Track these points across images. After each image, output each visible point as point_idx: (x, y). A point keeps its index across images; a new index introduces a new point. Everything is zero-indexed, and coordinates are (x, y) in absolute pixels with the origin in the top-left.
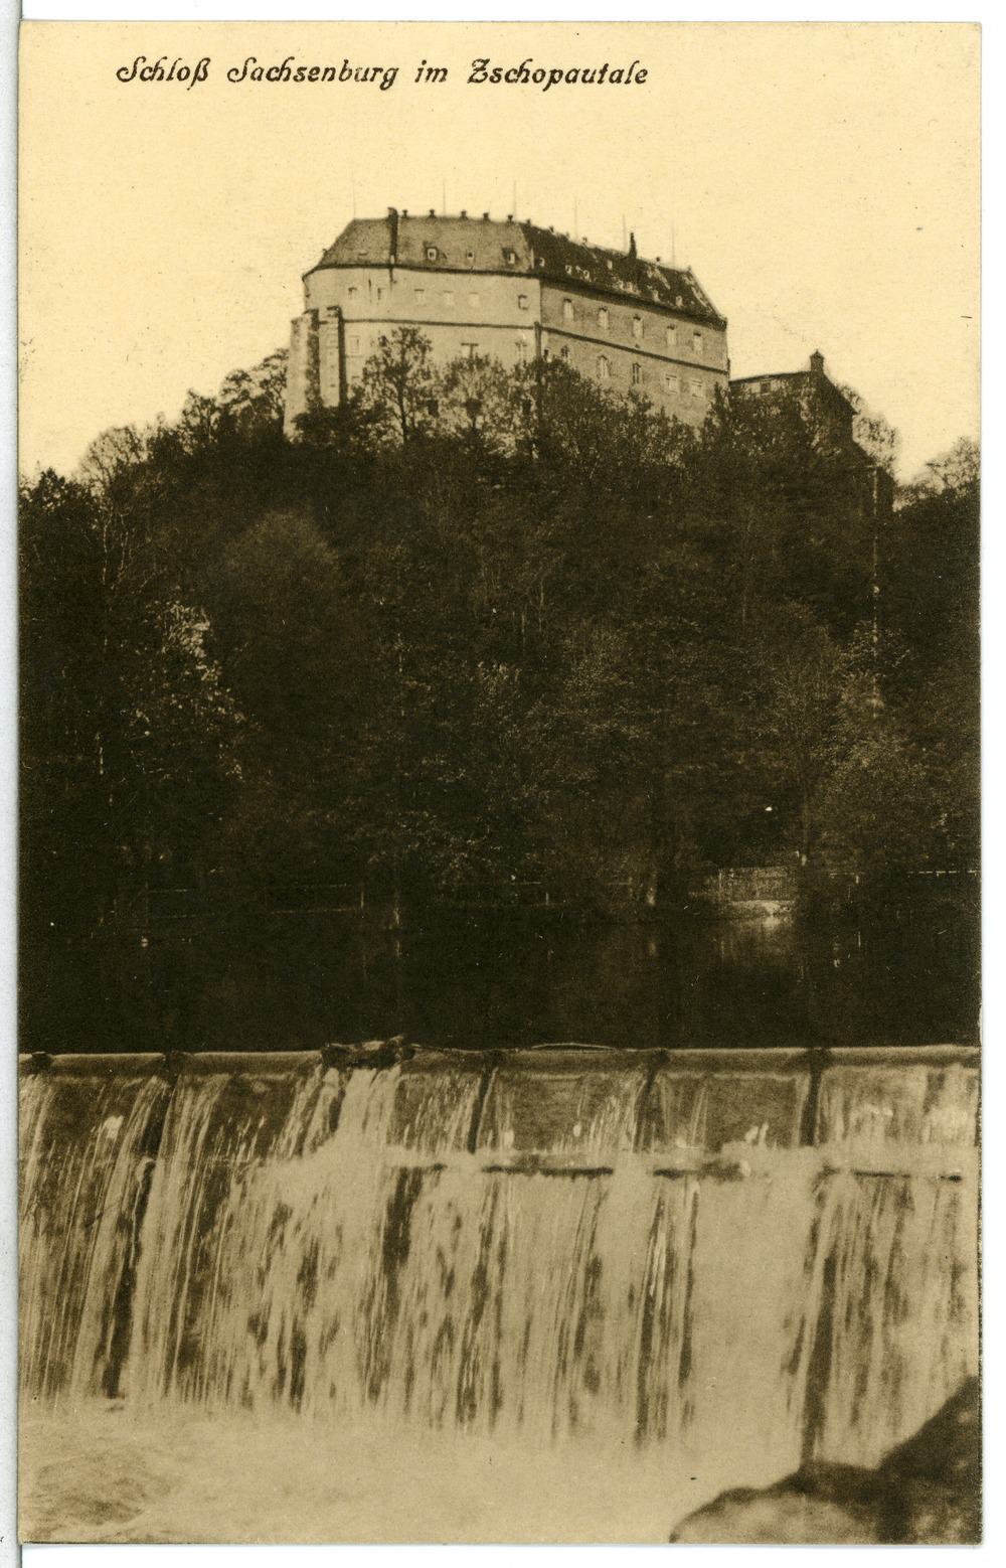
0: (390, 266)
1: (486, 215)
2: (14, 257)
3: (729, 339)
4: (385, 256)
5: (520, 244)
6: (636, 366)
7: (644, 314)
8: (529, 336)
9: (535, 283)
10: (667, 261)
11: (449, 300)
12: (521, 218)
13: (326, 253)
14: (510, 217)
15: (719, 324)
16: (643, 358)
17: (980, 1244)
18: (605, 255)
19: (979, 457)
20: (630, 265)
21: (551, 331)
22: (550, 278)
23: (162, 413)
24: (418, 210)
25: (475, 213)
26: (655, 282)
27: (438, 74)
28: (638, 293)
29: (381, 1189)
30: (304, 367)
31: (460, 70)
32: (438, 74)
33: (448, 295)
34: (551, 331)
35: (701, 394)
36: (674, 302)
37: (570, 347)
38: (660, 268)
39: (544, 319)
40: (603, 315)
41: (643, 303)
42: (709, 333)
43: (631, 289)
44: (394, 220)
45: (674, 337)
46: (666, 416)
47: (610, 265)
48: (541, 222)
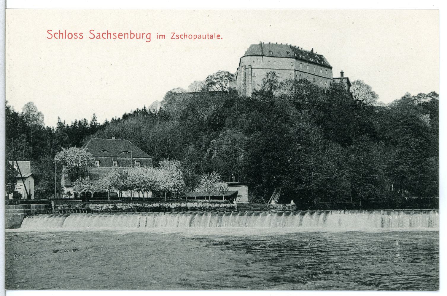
0: (263, 56)
1: (276, 43)
2: (4, 49)
3: (333, 72)
4: (261, 54)
5: (290, 51)
6: (314, 78)
7: (316, 66)
8: (293, 72)
9: (294, 60)
10: (318, 53)
11: (275, 63)
12: (289, 44)
13: (246, 52)
14: (287, 44)
15: (331, 68)
16: (316, 76)
17: (334, 288)
18: (306, 52)
19: (7, 198)
20: (312, 54)
21: (297, 71)
22: (297, 59)
23: (29, 103)
24: (266, 42)
25: (279, 43)
26: (316, 58)
27: (163, 36)
28: (314, 61)
29: (246, 240)
30: (243, 79)
31: (169, 36)
32: (163, 36)
33: (275, 63)
34: (297, 71)
35: (327, 84)
36: (321, 63)
37: (301, 74)
38: (317, 55)
39: (296, 68)
40: (308, 67)
41: (315, 63)
42: (329, 70)
43: (313, 60)
44: (261, 45)
45: (322, 71)
46: (146, 110)
47: (308, 55)
48: (293, 45)
